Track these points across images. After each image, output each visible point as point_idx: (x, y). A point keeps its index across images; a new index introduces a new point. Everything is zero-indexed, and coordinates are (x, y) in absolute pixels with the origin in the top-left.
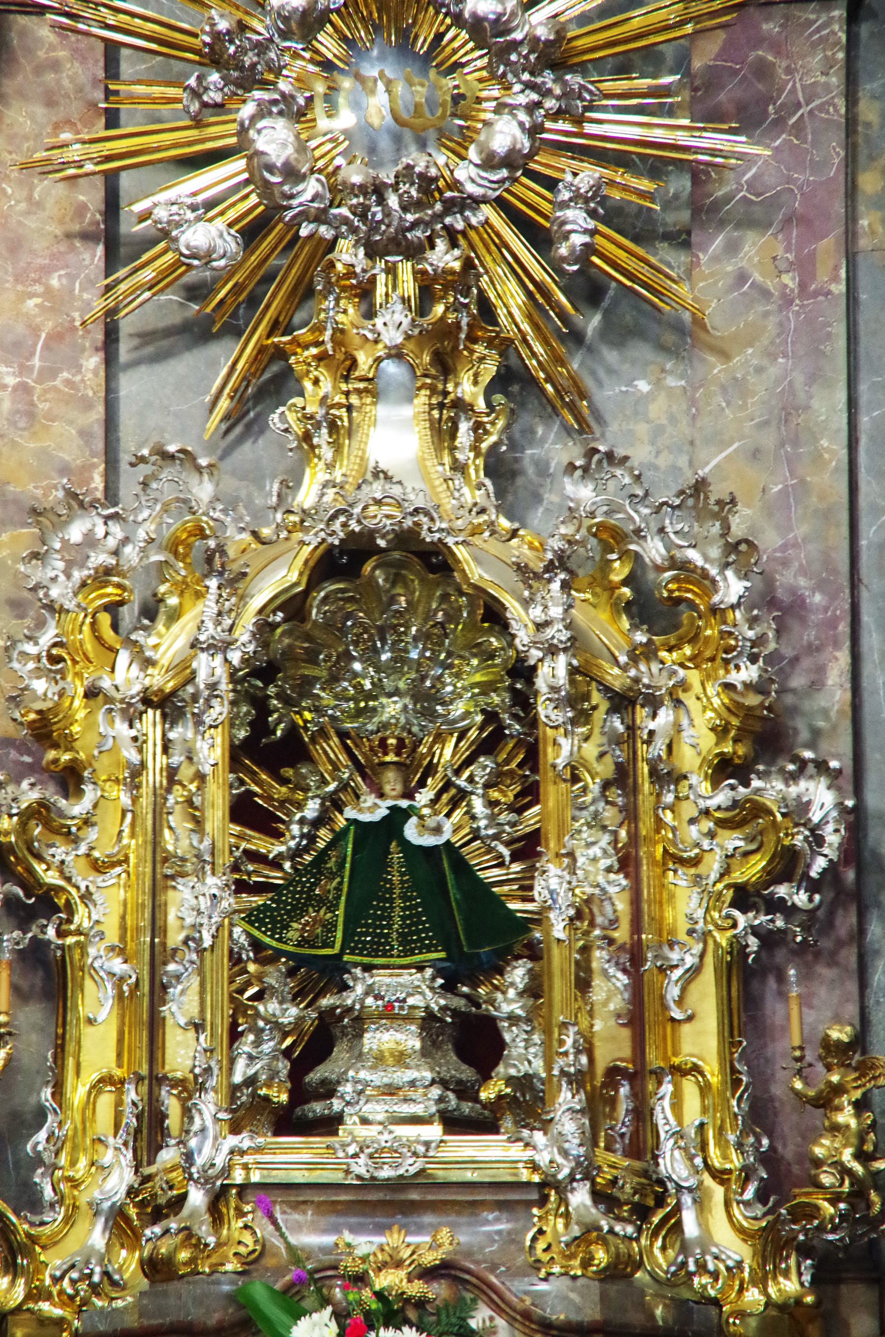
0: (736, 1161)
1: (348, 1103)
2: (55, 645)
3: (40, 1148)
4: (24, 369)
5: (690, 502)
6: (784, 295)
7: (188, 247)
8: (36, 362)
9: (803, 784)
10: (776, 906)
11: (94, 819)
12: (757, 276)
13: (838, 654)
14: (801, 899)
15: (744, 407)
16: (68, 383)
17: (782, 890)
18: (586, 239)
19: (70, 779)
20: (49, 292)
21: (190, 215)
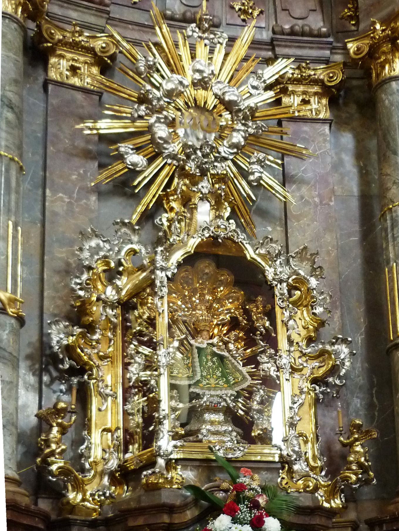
0: (319, 463)
1: (205, 436)
2: (88, 280)
3: (83, 451)
4: (70, 197)
5: (299, 255)
6: (315, 204)
7: (130, 162)
8: (75, 195)
9: (336, 347)
10: (327, 384)
11: (100, 341)
12: (307, 198)
13: (337, 312)
14: (338, 382)
15: (304, 235)
16: (85, 203)
17: (331, 379)
18: (260, 175)
19: (90, 328)
20: (79, 174)
21: (131, 152)
